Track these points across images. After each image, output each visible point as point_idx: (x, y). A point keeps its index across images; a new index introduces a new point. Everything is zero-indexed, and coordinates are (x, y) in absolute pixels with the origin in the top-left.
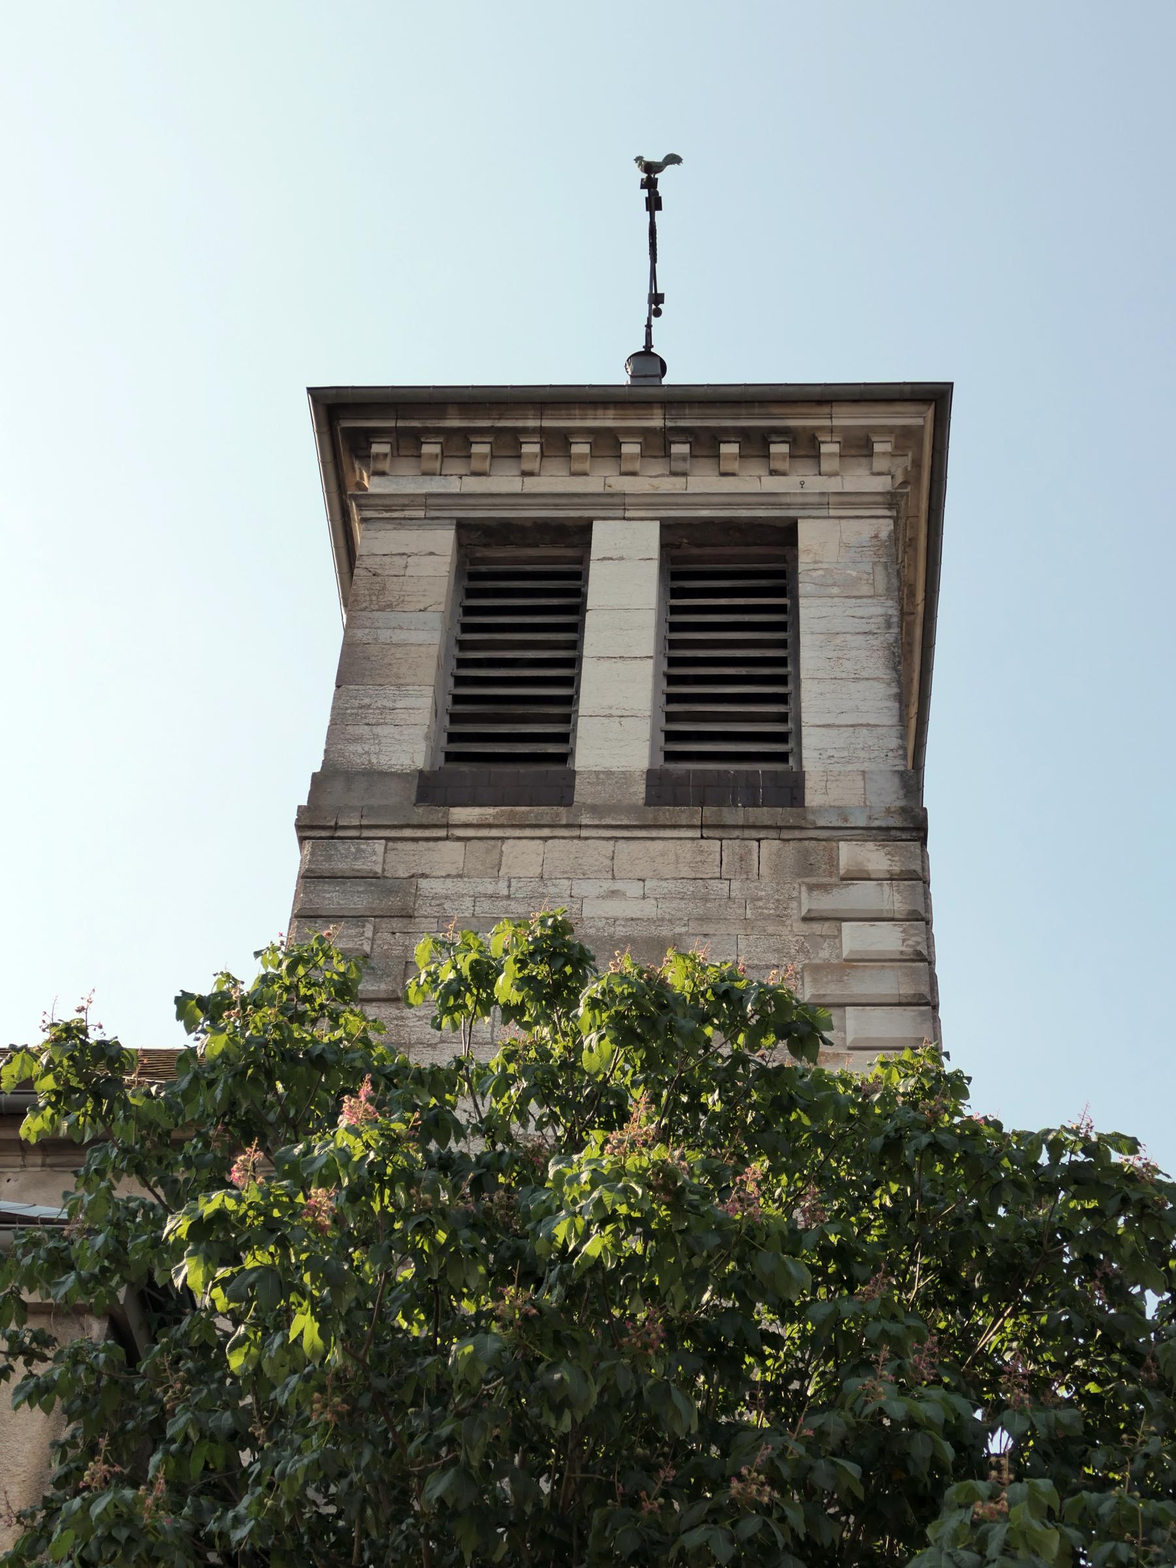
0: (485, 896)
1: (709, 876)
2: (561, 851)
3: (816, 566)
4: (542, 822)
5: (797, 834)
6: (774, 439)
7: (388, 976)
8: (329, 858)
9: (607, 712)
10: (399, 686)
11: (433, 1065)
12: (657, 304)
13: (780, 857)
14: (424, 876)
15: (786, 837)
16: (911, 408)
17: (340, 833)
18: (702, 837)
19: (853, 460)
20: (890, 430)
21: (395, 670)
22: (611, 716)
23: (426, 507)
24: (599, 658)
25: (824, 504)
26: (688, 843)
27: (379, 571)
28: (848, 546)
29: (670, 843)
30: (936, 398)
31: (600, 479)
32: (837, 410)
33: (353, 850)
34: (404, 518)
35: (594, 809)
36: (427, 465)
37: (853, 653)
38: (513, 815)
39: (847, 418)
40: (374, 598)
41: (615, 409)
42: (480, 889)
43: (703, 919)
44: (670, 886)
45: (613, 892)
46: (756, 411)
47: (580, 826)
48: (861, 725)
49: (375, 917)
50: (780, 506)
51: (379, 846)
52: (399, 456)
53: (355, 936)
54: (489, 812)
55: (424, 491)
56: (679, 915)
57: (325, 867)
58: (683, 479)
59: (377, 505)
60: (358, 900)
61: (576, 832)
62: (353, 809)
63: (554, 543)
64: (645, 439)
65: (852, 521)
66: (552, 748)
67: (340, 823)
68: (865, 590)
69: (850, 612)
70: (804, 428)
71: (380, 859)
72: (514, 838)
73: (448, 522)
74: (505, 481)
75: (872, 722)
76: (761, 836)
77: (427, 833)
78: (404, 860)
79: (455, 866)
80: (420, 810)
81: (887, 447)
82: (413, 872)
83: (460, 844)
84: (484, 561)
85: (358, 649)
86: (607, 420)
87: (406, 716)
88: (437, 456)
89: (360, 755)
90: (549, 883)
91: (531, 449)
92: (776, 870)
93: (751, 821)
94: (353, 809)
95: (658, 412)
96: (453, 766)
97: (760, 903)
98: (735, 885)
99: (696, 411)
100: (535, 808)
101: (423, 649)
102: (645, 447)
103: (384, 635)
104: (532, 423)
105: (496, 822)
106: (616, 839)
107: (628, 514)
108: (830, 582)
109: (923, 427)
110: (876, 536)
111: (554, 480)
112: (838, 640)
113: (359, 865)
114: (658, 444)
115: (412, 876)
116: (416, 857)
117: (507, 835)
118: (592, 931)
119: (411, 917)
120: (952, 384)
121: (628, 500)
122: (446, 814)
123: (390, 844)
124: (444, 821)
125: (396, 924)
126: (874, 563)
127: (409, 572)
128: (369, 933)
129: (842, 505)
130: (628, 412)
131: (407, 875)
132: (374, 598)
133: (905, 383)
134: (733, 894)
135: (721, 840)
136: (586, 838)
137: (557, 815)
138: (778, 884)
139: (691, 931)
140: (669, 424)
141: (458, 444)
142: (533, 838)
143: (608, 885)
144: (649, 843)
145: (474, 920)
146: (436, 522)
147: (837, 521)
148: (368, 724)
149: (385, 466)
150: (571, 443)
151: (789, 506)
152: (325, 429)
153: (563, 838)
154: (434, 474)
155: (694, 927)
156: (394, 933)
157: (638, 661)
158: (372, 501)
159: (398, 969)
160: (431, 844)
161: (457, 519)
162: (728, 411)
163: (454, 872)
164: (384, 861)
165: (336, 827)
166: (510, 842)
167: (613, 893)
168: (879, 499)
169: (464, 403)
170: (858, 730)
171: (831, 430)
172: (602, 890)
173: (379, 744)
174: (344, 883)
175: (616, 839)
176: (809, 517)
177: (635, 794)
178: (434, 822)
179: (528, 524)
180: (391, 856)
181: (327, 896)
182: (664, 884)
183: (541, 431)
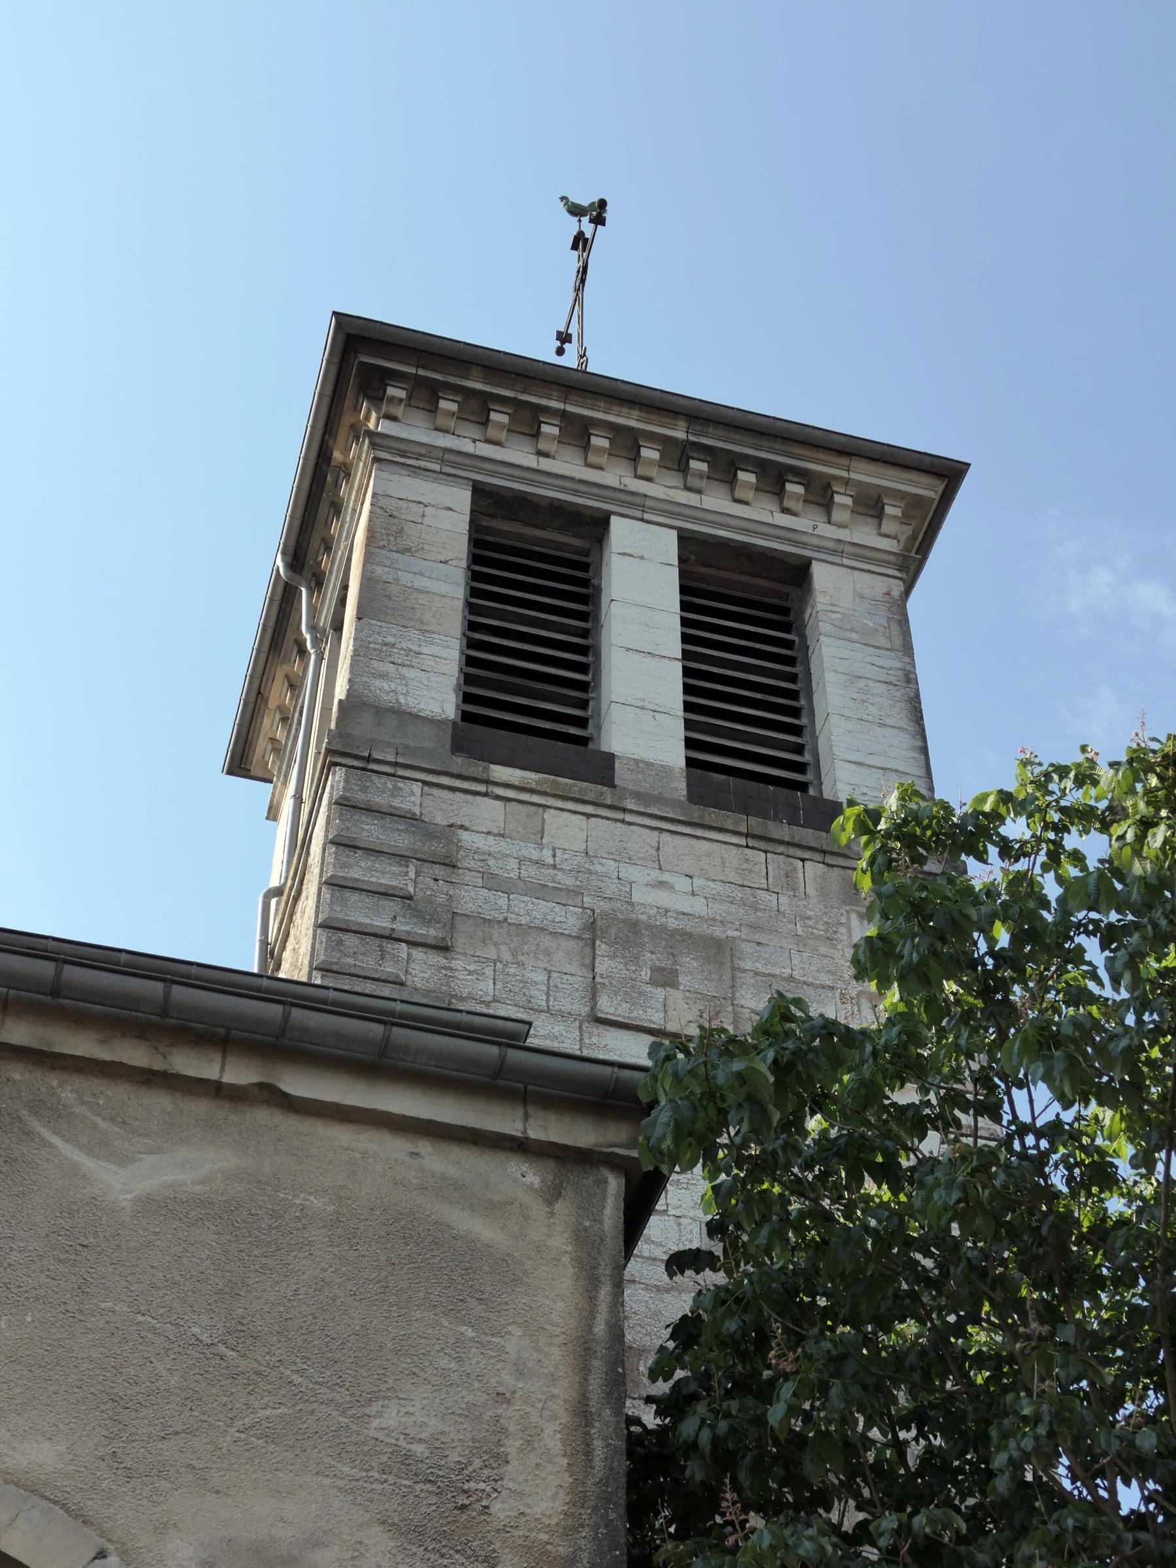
0: (530, 860)
1: (756, 886)
2: (606, 831)
3: (834, 609)
4: (586, 798)
5: (840, 861)
6: (790, 477)
7: (437, 922)
8: (365, 789)
9: (640, 703)
10: (424, 632)
12: (563, 342)
13: (825, 880)
14: (462, 827)
15: (830, 862)
17: (372, 766)
18: (747, 846)
20: (902, 495)
21: (418, 615)
22: (643, 708)
23: (443, 461)
24: (628, 649)
25: (838, 551)
26: (733, 849)
29: (715, 846)
32: (857, 464)
33: (390, 785)
34: (419, 468)
35: (637, 795)
36: (441, 421)
37: (877, 699)
38: (557, 785)
39: (864, 474)
40: (392, 539)
41: (640, 411)
42: (524, 852)
43: (755, 927)
44: (718, 888)
45: (661, 883)
46: (778, 446)
47: (624, 810)
48: (890, 769)
49: (418, 859)
50: (797, 543)
51: (417, 788)
52: (409, 405)
53: (399, 875)
54: (532, 777)
55: (443, 445)
56: (730, 918)
57: (360, 797)
58: (697, 497)
59: (392, 448)
60: (401, 841)
61: (620, 816)
62: (388, 745)
63: (561, 529)
66: (572, 730)
67: (376, 755)
68: (883, 642)
69: (868, 659)
70: (822, 474)
71: (418, 802)
72: (556, 808)
74: (519, 454)
75: (900, 769)
76: (806, 856)
78: (442, 808)
80: (459, 760)
82: (451, 821)
83: (498, 804)
85: (379, 586)
86: (630, 419)
87: (433, 664)
88: (454, 414)
89: (388, 693)
90: (596, 861)
92: (823, 892)
93: (797, 840)
94: (388, 745)
95: (683, 424)
97: (810, 923)
98: (784, 899)
100: (579, 783)
103: (405, 578)
104: (554, 404)
105: (539, 788)
106: (661, 830)
107: (646, 516)
108: (849, 627)
110: (888, 594)
112: (861, 684)
113: (396, 803)
114: (677, 458)
115: (451, 826)
116: (454, 807)
117: (549, 804)
118: (644, 918)
119: (454, 866)
120: (969, 465)
122: (486, 770)
123: (426, 788)
124: (484, 776)
125: (439, 871)
126: (889, 619)
127: (426, 521)
128: (412, 875)
129: (855, 556)
130: (653, 417)
132: (392, 539)
133: (926, 454)
134: (782, 909)
135: (766, 852)
136: (630, 824)
137: (602, 794)
138: (826, 907)
139: (743, 937)
140: (692, 438)
142: (575, 812)
143: (655, 874)
144: (694, 841)
145: (521, 883)
147: (850, 571)
148: (393, 663)
149: (399, 411)
152: (336, 360)
153: (607, 818)
154: (447, 432)
155: (745, 933)
157: (667, 660)
158: (386, 442)
159: (446, 917)
160: (469, 797)
161: (474, 481)
162: (751, 440)
163: (496, 831)
165: (369, 759)
166: (552, 811)
167: (661, 884)
168: (892, 558)
169: (491, 368)
170: (888, 773)
171: (847, 482)
172: (649, 878)
175: (661, 830)
176: (823, 561)
177: (676, 789)
178: (474, 775)
179: (544, 503)
180: (428, 801)
181: (366, 827)
182: (712, 885)
183: (564, 414)
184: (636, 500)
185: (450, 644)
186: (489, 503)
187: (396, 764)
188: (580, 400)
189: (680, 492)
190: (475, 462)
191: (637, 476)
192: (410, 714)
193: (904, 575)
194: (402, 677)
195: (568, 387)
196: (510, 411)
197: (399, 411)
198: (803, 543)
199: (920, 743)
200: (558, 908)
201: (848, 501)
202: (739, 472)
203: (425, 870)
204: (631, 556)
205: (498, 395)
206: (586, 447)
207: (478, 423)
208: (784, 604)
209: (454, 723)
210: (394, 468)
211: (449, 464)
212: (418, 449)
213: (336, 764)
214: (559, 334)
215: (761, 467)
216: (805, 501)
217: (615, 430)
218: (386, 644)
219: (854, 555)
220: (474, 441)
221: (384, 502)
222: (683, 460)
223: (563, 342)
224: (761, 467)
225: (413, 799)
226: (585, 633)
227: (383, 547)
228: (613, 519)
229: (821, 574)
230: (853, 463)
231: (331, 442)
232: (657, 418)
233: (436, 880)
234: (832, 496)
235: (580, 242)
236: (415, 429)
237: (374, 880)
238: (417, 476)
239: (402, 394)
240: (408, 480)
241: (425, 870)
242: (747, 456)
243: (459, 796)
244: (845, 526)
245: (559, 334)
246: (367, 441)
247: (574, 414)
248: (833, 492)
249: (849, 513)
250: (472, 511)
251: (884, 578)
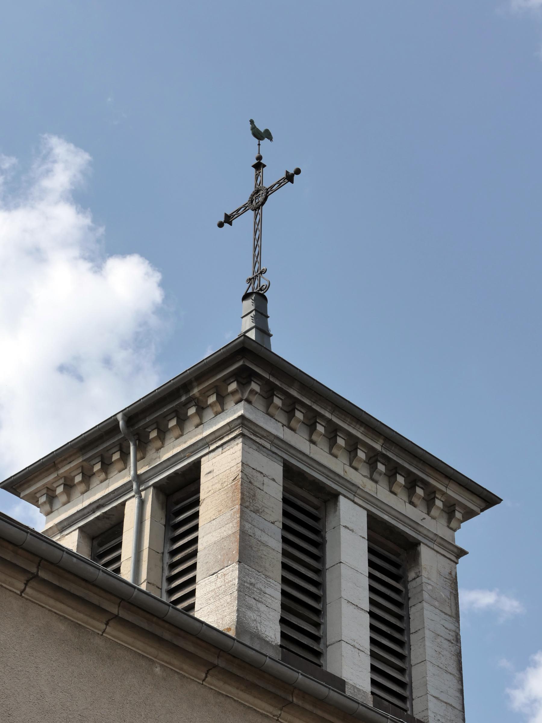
10: (267, 576)
23: (272, 443)
31: (358, 477)
32: (452, 486)
39: (453, 492)
41: (365, 428)
59: (251, 429)
65: (442, 557)
86: (357, 432)
87: (270, 601)
88: (279, 407)
95: (381, 441)
104: (328, 415)
107: (356, 500)
111: (338, 465)
129: (440, 545)
140: (384, 452)
146: (274, 455)
148: (254, 599)
151: (419, 533)
158: (249, 425)
168: (455, 550)
171: (443, 494)
194: (259, 611)
195: (336, 406)
196: (304, 412)
198: (420, 532)
199: (460, 687)
204: (348, 528)
209: (281, 646)
217: (349, 435)
219: (440, 544)
221: (248, 470)
242: (405, 468)
247: (335, 422)
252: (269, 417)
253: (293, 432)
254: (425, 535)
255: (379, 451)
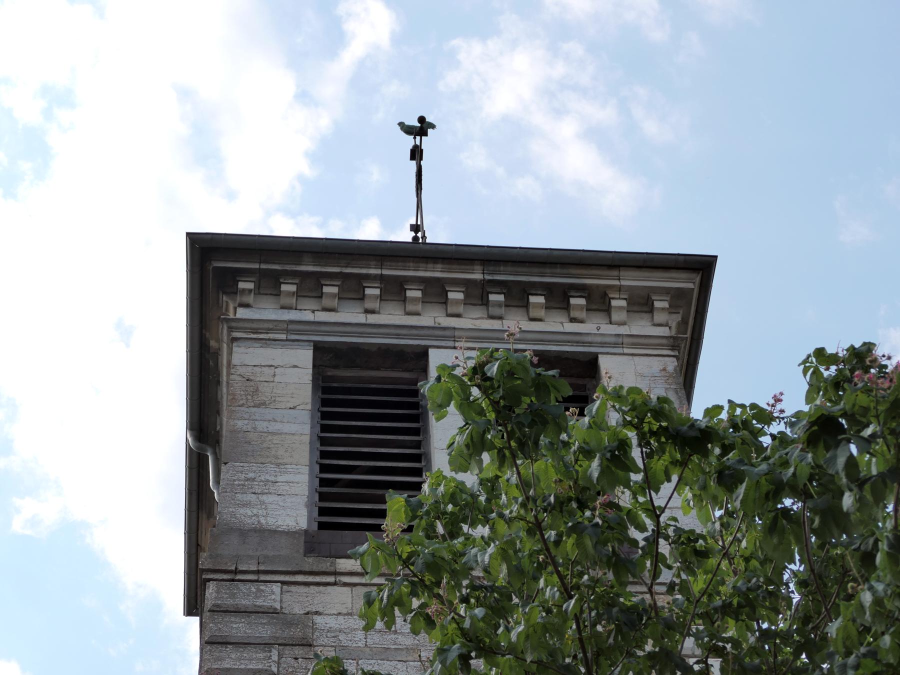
6: (572, 294)
8: (233, 596)
10: (278, 465)
11: (847, 350)
14: (317, 613)
16: (683, 275)
19: (636, 314)
20: (666, 291)
21: (273, 453)
23: (287, 331)
25: (617, 344)
27: (252, 378)
28: (642, 376)
30: (703, 267)
32: (623, 273)
33: (253, 589)
34: (269, 340)
39: (632, 280)
40: (250, 397)
41: (443, 263)
46: (558, 271)
49: (279, 645)
50: (583, 344)
51: (276, 588)
52: (259, 294)
53: (264, 659)
58: (499, 322)
59: (246, 328)
60: (264, 630)
62: (251, 557)
63: (392, 368)
64: (467, 289)
65: (643, 358)
67: (240, 568)
70: (598, 286)
71: (278, 598)
73: (306, 343)
74: (351, 315)
77: (318, 579)
78: (297, 601)
79: (344, 606)
80: (310, 560)
81: (665, 305)
82: (307, 610)
84: (333, 379)
85: (240, 435)
86: (436, 272)
87: (287, 488)
89: (251, 517)
91: (372, 291)
94: (251, 557)
95: (478, 268)
96: (326, 533)
99: (509, 269)
101: (296, 437)
102: (467, 295)
103: (262, 426)
104: (373, 271)
109: (693, 289)
110: (664, 370)
111: (392, 315)
113: (259, 602)
114: (478, 295)
115: (308, 613)
116: (309, 598)
119: (310, 645)
120: (716, 257)
121: (457, 333)
123: (285, 587)
124: (332, 569)
125: (298, 651)
126: (666, 389)
127: (277, 379)
130: (454, 267)
131: (302, 612)
132: (250, 397)
140: (488, 277)
141: (311, 287)
145: (368, 650)
146: (296, 343)
147: (631, 357)
148: (254, 493)
149: (250, 299)
150: (406, 289)
151: (590, 344)
154: (291, 308)
156: (296, 659)
158: (241, 325)
160: (321, 588)
161: (314, 341)
162: (535, 270)
163: (345, 611)
164: (281, 601)
165: (236, 572)
168: (664, 341)
171: (620, 289)
173: (266, 509)
174: (249, 617)
176: (608, 353)
178: (323, 570)
180: (287, 597)
181: (234, 626)
183: (381, 278)
184: (447, 333)
185: (300, 470)
186: (327, 357)
187: (258, 572)
188: (394, 264)
189: (485, 321)
190: (313, 328)
191: (449, 315)
192: (270, 530)
193: (676, 353)
196: (338, 283)
197: (250, 299)
200: (400, 665)
201: (623, 303)
202: (530, 297)
203: (287, 652)
205: (326, 272)
206: (445, 302)
207: (316, 297)
208: (583, 394)
210: (249, 343)
211: (292, 332)
212: (266, 326)
213: (209, 580)
214: (412, 226)
215: (549, 290)
216: (588, 310)
218: (248, 480)
219: (633, 344)
220: (313, 312)
222: (485, 294)
223: (416, 231)
224: (549, 290)
225: (273, 597)
226: (418, 445)
227: (242, 405)
228: (431, 351)
229: (605, 363)
230: (622, 273)
231: (208, 335)
232: (458, 267)
233: (296, 659)
234: (610, 302)
235: (416, 154)
236: (266, 311)
237: (243, 667)
238: (268, 346)
239: (251, 286)
240: (262, 350)
241: (287, 652)
243: (313, 589)
244: (624, 324)
245: (412, 226)
246: (225, 327)
248: (610, 299)
249: (625, 312)
250: (314, 366)
251: (660, 358)
252: (286, 311)
253: (333, 313)
254: (601, 343)
255: (481, 280)
